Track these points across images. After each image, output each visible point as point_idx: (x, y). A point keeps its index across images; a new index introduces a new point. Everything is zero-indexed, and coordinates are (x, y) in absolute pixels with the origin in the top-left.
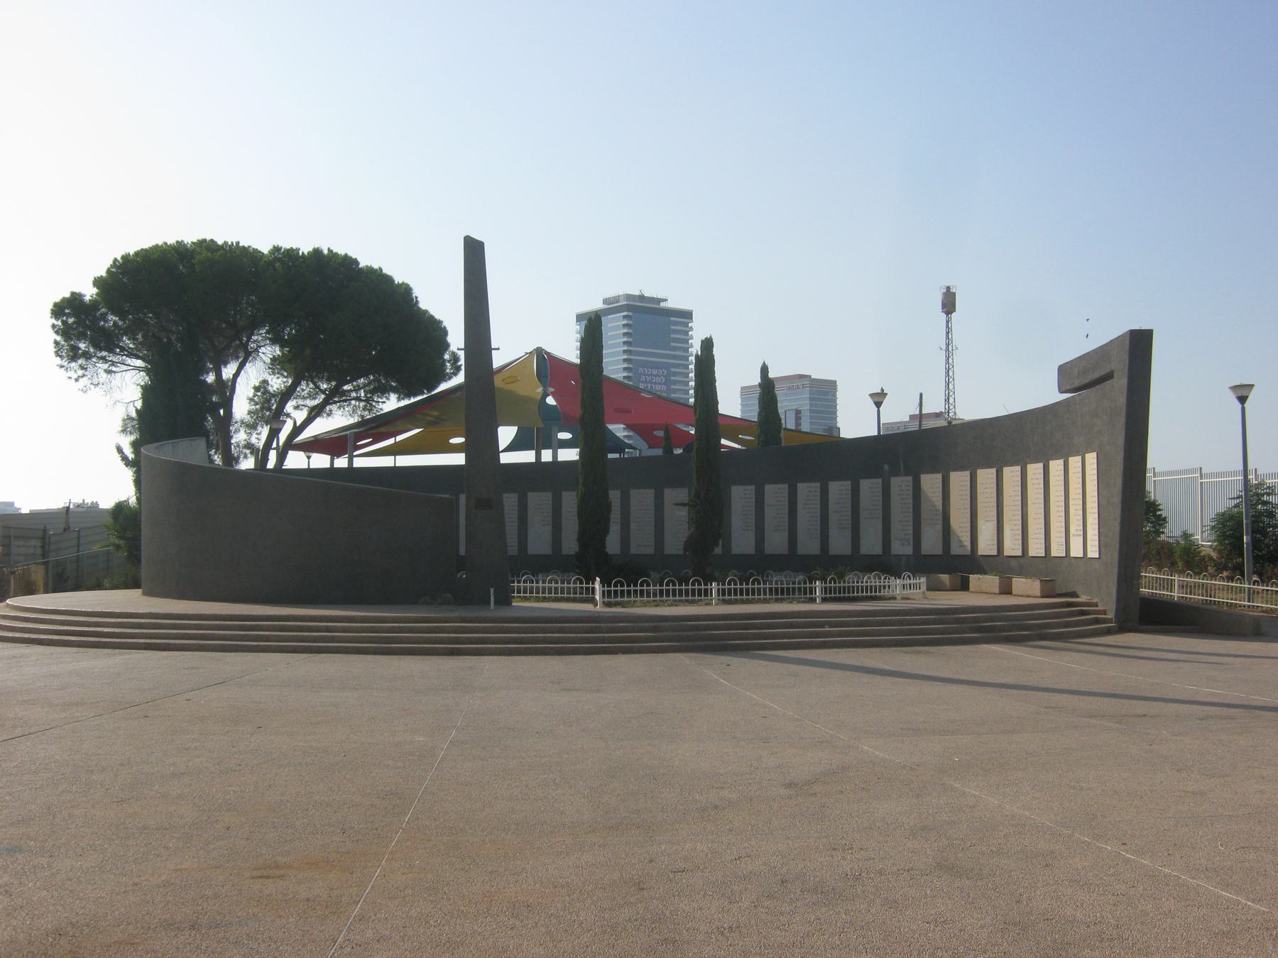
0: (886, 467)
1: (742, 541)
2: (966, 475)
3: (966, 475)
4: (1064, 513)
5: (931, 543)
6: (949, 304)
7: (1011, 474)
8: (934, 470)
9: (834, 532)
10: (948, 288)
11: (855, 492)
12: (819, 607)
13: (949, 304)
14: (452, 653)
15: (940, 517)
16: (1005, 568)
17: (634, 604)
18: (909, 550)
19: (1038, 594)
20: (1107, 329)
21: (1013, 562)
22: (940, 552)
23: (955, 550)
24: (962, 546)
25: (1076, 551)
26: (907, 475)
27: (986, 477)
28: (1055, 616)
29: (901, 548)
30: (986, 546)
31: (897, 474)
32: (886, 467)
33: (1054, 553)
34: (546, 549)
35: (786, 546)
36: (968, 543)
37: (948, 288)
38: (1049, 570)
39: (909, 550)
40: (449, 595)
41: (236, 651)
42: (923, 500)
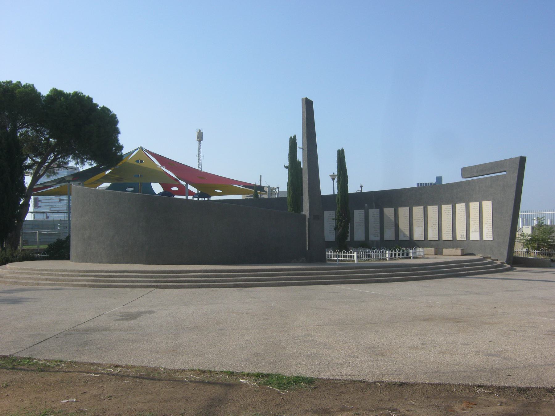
0: (366, 205)
1: (359, 235)
2: (407, 209)
3: (407, 209)
4: (477, 222)
5: (389, 235)
6: (200, 137)
7: (460, 207)
8: (390, 207)
9: (371, 231)
10: (200, 130)
11: (382, 214)
12: (388, 262)
13: (200, 137)
14: (199, 287)
15: (394, 224)
16: (438, 246)
17: (18, 269)
18: (378, 239)
19: (460, 254)
20: (517, 154)
21: (433, 243)
22: (394, 239)
23: (401, 238)
24: (405, 235)
25: (475, 236)
26: (376, 208)
27: (446, 209)
28: (471, 265)
29: (374, 237)
30: (418, 235)
31: (372, 208)
32: (366, 205)
33: (459, 238)
34: (363, 238)
35: (394, 236)
36: (408, 234)
37: (200, 130)
38: (466, 247)
39: (378, 239)
40: (304, 258)
41: (430, 279)
42: (385, 217)
